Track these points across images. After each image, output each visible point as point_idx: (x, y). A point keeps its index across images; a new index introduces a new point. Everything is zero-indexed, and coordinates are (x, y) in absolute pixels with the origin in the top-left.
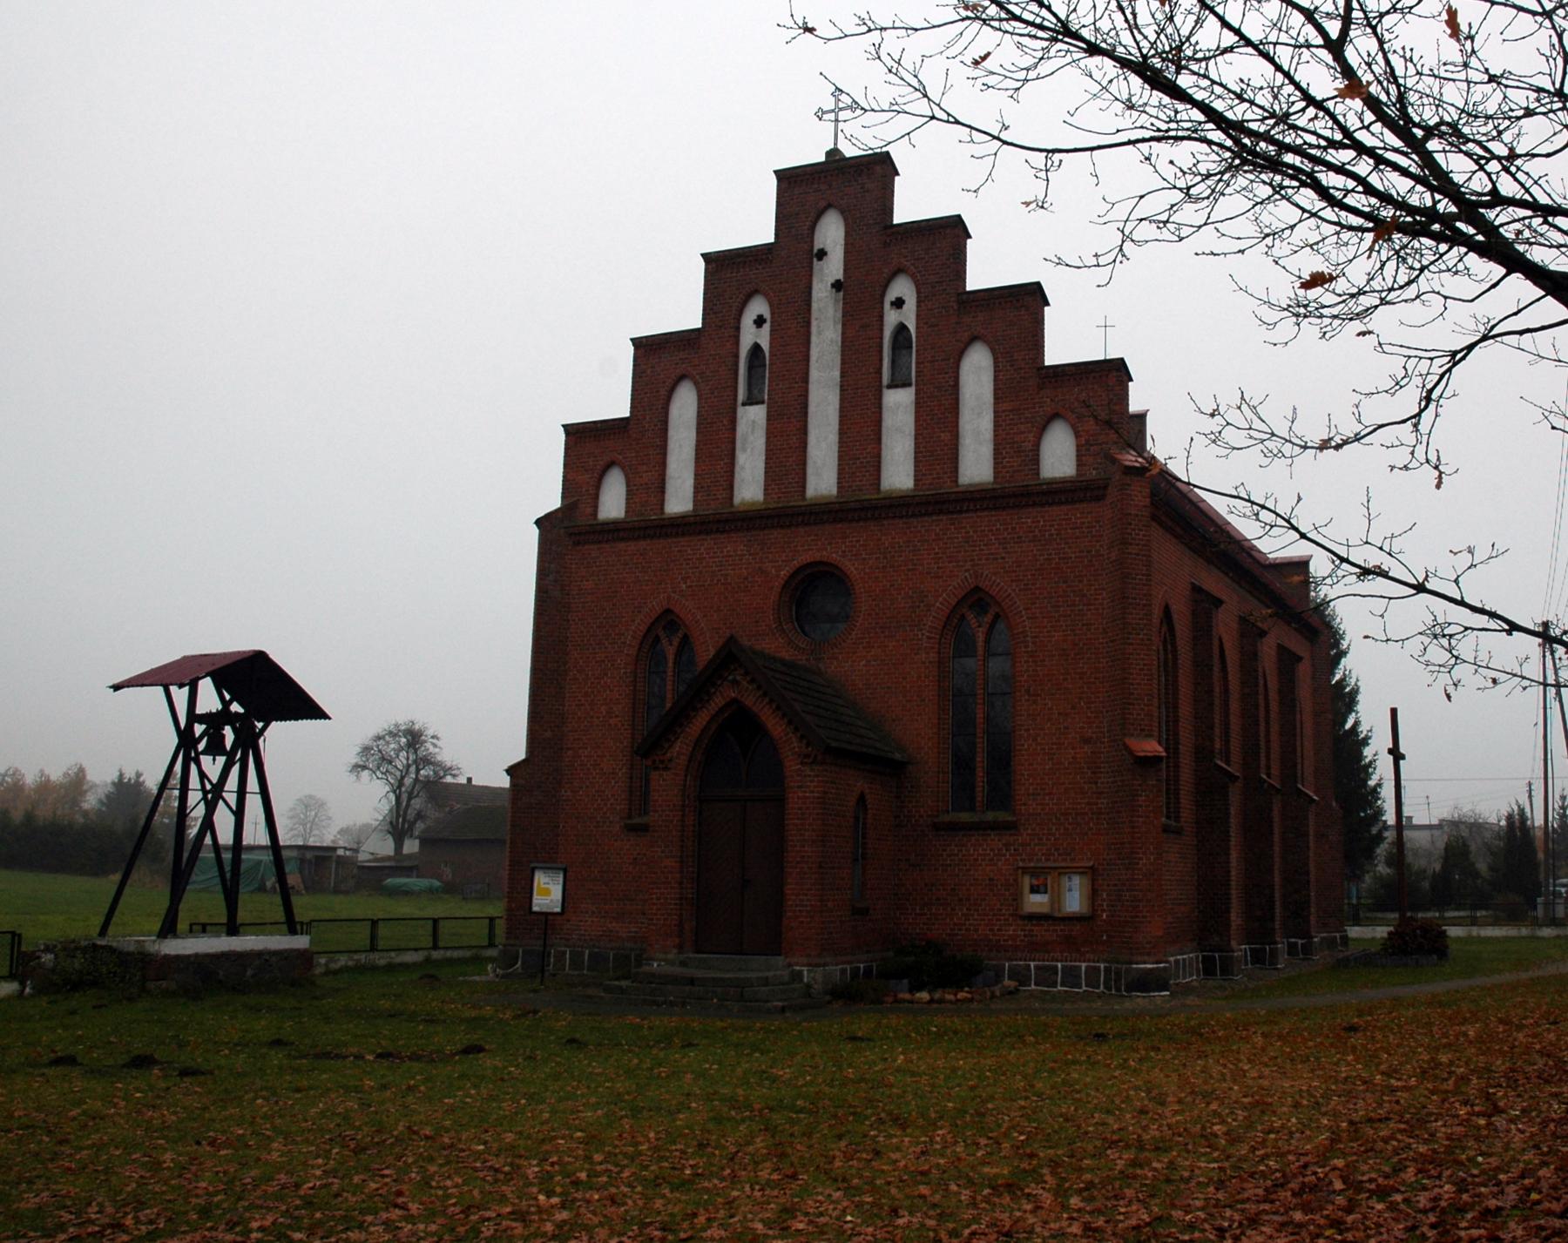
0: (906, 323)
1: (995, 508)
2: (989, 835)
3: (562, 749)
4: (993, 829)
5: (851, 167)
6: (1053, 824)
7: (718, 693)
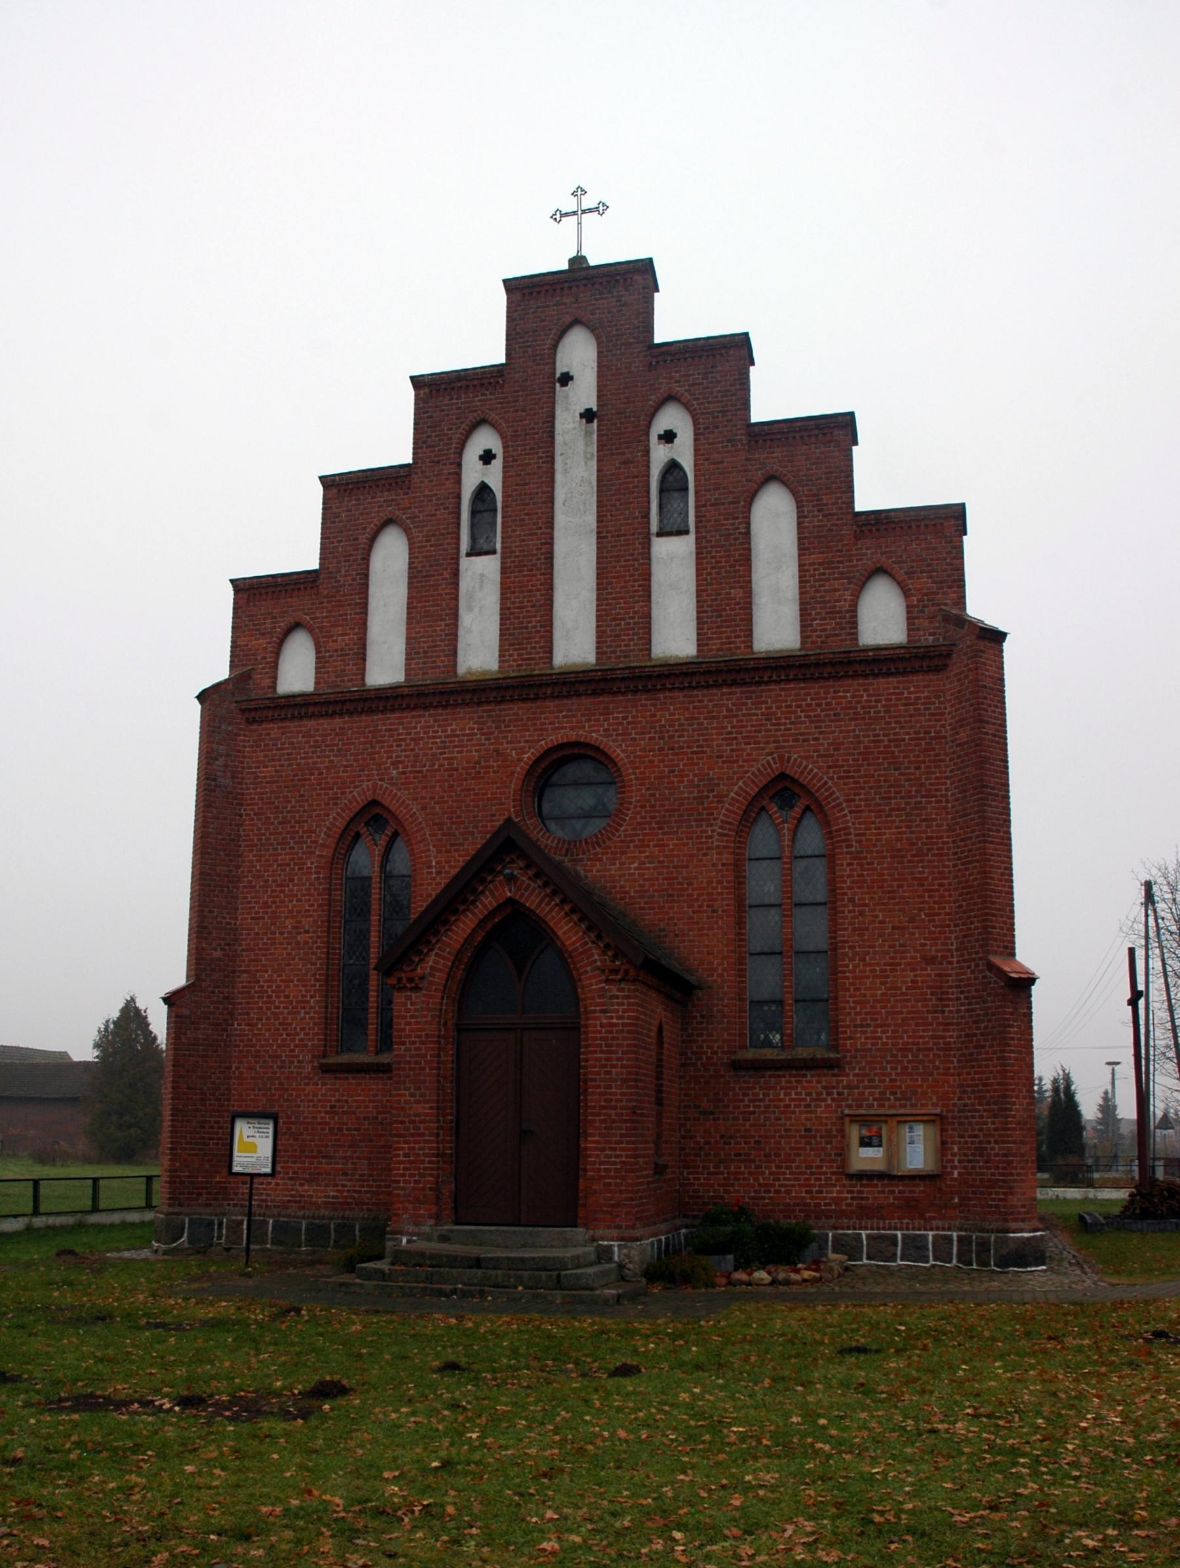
0: (679, 460)
1: (804, 680)
2: (805, 1076)
3: (234, 972)
4: (808, 1068)
6: (888, 1062)
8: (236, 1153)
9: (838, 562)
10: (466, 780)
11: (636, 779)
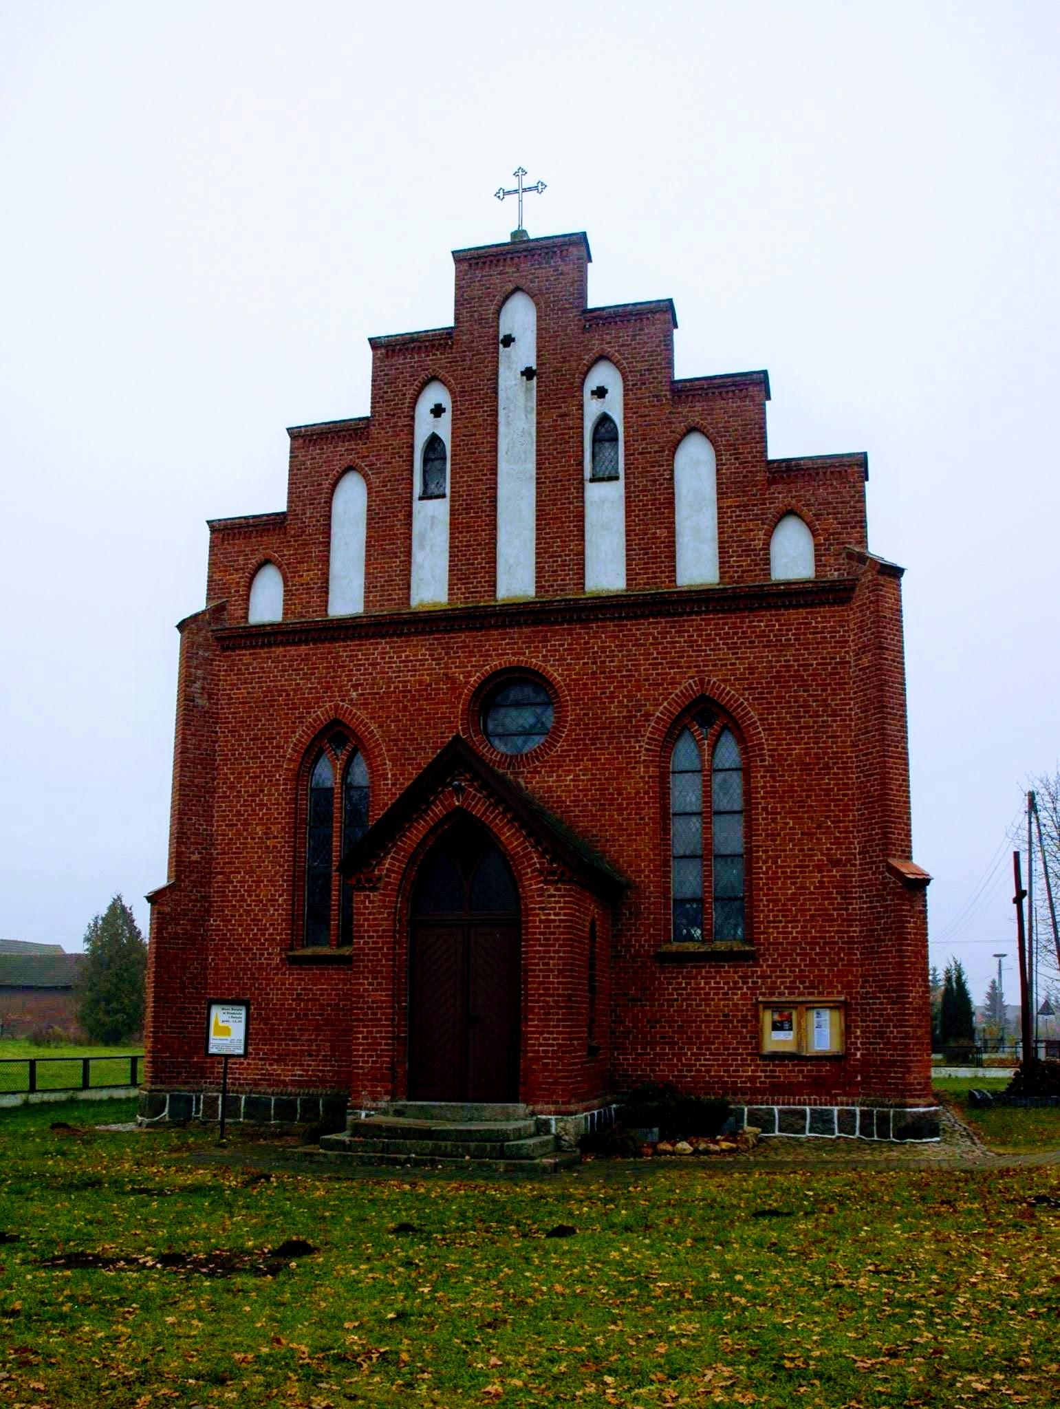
0: (610, 413)
6: (798, 954)
10: (418, 701)
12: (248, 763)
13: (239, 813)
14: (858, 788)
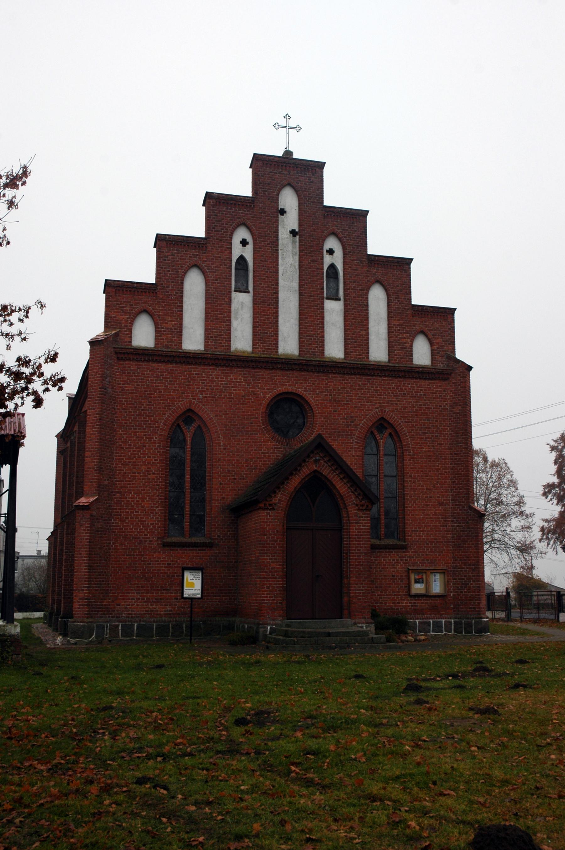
0: (336, 264)
1: (392, 377)
2: (392, 552)
4: (393, 549)
5: (303, 165)
6: (425, 547)
7: (305, 467)
8: (185, 588)
9: (405, 326)
10: (238, 404)
11: (319, 413)
12: (136, 429)
13: (130, 458)
14: (452, 469)
